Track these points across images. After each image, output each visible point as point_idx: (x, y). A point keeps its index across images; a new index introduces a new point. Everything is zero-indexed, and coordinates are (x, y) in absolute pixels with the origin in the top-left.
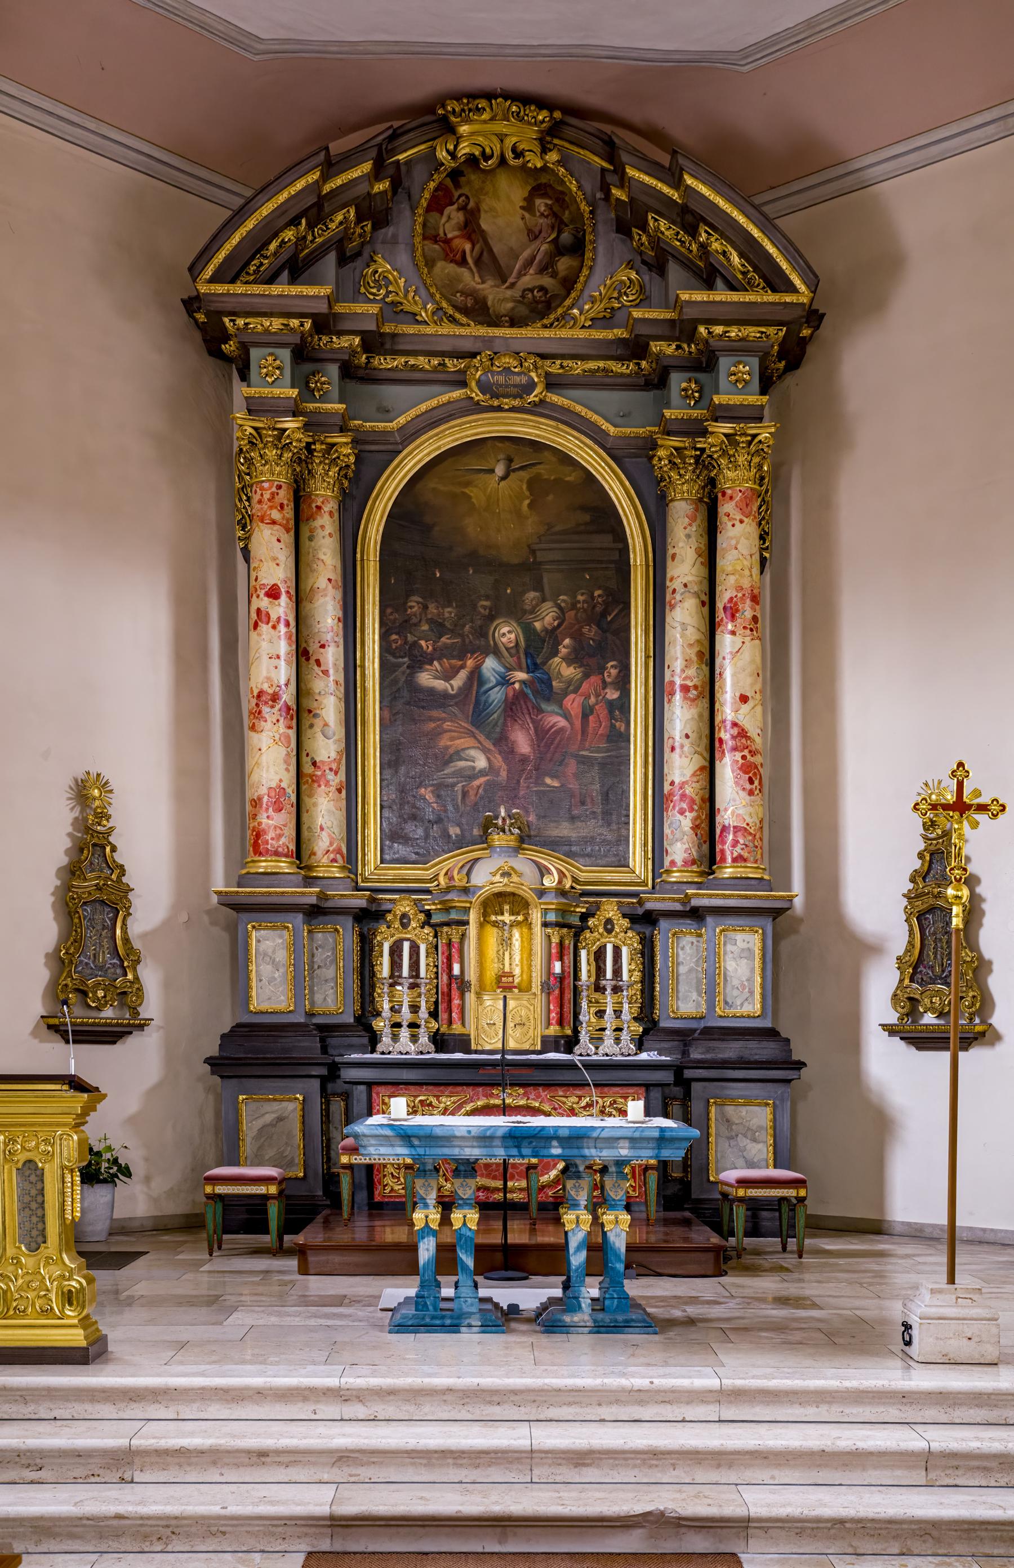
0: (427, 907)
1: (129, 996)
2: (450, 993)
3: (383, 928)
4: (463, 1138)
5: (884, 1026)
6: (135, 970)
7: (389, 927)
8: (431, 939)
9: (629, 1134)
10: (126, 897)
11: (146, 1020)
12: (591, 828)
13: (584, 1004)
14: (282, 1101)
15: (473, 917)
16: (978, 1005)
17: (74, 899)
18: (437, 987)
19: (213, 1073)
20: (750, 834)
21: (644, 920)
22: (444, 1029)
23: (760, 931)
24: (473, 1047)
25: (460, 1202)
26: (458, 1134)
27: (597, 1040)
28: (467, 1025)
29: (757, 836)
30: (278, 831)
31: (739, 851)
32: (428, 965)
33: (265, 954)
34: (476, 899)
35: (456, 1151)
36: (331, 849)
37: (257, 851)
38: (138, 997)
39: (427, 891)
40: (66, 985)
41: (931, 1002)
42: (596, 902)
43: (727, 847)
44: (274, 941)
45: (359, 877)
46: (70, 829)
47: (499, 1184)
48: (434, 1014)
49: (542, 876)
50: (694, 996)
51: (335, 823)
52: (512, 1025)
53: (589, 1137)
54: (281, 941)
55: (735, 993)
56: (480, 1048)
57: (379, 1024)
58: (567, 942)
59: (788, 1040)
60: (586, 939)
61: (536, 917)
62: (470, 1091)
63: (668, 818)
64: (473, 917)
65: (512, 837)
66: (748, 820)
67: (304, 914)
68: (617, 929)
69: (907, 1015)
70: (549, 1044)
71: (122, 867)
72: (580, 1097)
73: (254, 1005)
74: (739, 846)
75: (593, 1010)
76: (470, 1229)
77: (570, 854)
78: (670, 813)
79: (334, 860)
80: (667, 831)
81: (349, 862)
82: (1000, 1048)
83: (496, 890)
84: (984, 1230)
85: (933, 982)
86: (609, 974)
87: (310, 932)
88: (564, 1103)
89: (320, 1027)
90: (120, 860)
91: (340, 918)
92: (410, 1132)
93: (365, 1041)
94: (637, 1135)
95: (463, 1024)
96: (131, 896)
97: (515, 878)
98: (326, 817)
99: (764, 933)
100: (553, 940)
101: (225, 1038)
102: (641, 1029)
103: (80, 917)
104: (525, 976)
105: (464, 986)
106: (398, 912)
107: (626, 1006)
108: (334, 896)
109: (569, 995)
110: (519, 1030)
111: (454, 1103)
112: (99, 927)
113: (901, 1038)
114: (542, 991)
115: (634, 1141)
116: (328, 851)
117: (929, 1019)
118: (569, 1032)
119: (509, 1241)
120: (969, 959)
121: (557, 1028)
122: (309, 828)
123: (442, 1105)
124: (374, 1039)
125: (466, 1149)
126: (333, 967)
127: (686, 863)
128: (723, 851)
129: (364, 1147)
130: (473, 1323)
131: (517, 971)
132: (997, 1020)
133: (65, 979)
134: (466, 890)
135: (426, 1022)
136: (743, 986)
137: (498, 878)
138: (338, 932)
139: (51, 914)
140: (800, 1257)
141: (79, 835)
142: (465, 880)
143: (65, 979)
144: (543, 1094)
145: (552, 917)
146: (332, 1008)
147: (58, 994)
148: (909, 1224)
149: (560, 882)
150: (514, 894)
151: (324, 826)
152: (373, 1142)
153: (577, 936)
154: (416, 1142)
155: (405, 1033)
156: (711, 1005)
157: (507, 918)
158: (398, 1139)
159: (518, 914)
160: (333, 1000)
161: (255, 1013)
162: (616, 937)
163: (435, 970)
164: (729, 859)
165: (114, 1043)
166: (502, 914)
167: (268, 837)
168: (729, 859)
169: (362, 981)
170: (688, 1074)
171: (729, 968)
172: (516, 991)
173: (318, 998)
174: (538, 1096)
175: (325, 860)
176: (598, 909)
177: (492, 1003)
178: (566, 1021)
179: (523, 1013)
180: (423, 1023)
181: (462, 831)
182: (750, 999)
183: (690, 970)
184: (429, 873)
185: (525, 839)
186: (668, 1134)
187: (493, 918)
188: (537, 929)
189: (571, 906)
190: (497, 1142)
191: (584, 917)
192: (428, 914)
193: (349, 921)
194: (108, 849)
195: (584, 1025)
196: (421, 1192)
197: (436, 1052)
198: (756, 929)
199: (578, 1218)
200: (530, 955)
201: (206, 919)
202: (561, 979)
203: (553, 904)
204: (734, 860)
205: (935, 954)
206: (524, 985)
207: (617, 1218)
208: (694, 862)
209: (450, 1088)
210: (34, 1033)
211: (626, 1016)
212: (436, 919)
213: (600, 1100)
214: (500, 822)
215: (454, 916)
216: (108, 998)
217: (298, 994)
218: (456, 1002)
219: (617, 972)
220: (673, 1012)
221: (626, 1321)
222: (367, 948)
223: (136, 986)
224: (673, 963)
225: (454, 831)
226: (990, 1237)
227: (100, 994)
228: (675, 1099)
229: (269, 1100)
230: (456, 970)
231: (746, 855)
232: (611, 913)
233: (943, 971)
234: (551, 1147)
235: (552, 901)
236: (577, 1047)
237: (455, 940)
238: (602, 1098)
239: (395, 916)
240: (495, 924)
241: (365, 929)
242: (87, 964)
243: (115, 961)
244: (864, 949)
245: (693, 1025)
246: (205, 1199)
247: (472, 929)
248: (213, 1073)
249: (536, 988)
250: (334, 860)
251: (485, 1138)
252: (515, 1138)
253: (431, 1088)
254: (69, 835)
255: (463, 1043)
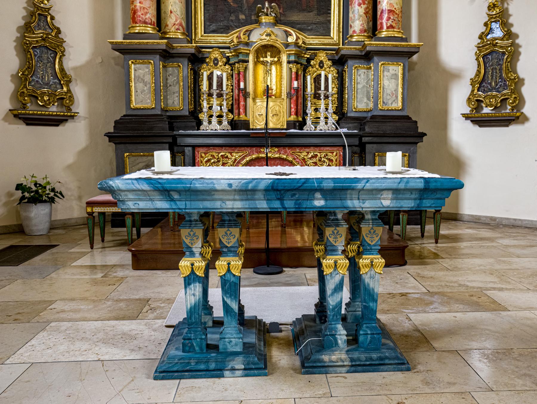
0: (227, 55)
1: (66, 101)
2: (239, 98)
3: (205, 66)
4: (223, 191)
5: (464, 115)
6: (68, 86)
7: (208, 65)
8: (229, 71)
9: (395, 186)
10: (62, 46)
11: (74, 113)
12: (311, 17)
13: (309, 104)
14: (148, 156)
15: (251, 58)
16: (517, 102)
17: (27, 44)
18: (233, 97)
19: (110, 141)
20: (396, 14)
21: (340, 61)
22: (236, 118)
23: (402, 65)
24: (251, 127)
25: (225, 250)
26: (218, 187)
27: (316, 123)
28: (248, 115)
29: (400, 15)
30: (146, 10)
31: (391, 23)
32: (227, 85)
33: (139, 77)
34: (253, 48)
35: (218, 204)
36: (176, 23)
37: (135, 22)
38: (70, 101)
39: (228, 48)
40: (23, 92)
41: (490, 101)
42: (314, 53)
43: (384, 21)
44: (144, 70)
45: (193, 41)
46: (25, 5)
47: (269, 155)
48: (231, 111)
49: (287, 37)
50: (365, 100)
51: (178, 9)
52: (271, 115)
53: (353, 189)
54: (147, 70)
55: (389, 97)
56: (254, 127)
57: (203, 117)
58: (300, 73)
59: (416, 122)
60: (309, 71)
61: (284, 58)
62: (248, 150)
63: (352, 8)
64: (251, 58)
65: (272, 17)
66: (396, 6)
67: (160, 56)
68: (325, 66)
69: (475, 109)
70: (291, 124)
71: (58, 29)
72: (308, 153)
73: (133, 105)
74: (391, 20)
75: (313, 108)
76: (234, 275)
77: (300, 30)
78: (353, 6)
79: (178, 29)
80: (351, 15)
81: (188, 31)
82: (527, 125)
83: (263, 44)
84: (515, 220)
85: (491, 90)
86: (323, 88)
87: (164, 67)
88: (299, 156)
89: (170, 117)
90: (57, 25)
91: (181, 59)
92: (167, 186)
93: (194, 124)
94: (402, 186)
95: (246, 115)
96: (64, 45)
97: (273, 37)
98: (173, 6)
99: (404, 66)
100: (293, 71)
101: (117, 123)
102: (337, 118)
103: (31, 55)
104: (278, 90)
105: (246, 95)
106: (212, 57)
107: (330, 105)
108: (177, 46)
109: (300, 100)
110: (275, 117)
111: (240, 156)
112: (45, 61)
113: (472, 121)
114: (287, 97)
115: (397, 192)
116: (175, 24)
117: (487, 110)
118: (300, 119)
119: (271, 246)
120: (512, 78)
121: (295, 116)
122: (165, 12)
123: (233, 158)
124: (199, 123)
125: (227, 202)
126: (178, 85)
127: (361, 31)
128: (381, 24)
129: (123, 201)
130: (237, 367)
131: (274, 87)
132: (526, 110)
133: (22, 89)
134: (247, 44)
135: (227, 115)
136: (392, 93)
137: (264, 37)
138: (180, 67)
139: (14, 53)
140: (437, 242)
141: (32, 9)
142: (247, 39)
143: (22, 89)
144: (288, 151)
145: (292, 58)
146: (177, 108)
147: (19, 96)
148: (472, 216)
149: (297, 40)
150: (272, 46)
151: (172, 10)
152: (131, 196)
153: (304, 71)
154: (176, 196)
155: (214, 120)
156: (376, 104)
157: (269, 59)
158: (155, 193)
159: (275, 57)
160: (178, 102)
161: (134, 109)
162: (325, 70)
163: (231, 88)
164: (385, 27)
165: (58, 125)
166: (267, 57)
167: (139, 13)
168: (385, 27)
169: (195, 94)
170: (365, 139)
171: (385, 84)
172: (274, 97)
173: (170, 102)
174: (286, 152)
175: (173, 29)
176: (316, 56)
177: (261, 104)
178: (299, 114)
179: (277, 109)
180: (225, 114)
181: (246, 16)
182: (396, 101)
183: (364, 87)
184: (228, 40)
185: (277, 22)
186: (432, 185)
187: (262, 59)
188: (285, 64)
189: (302, 53)
190: (260, 195)
191: (309, 60)
192: (228, 58)
193: (186, 61)
194: (49, 19)
195: (309, 115)
196: (187, 241)
197: (232, 129)
198: (400, 63)
199: (336, 262)
200: (281, 78)
201: (112, 62)
202: (297, 90)
203: (293, 51)
204: (388, 28)
205: (492, 76)
206: (278, 95)
207: (372, 262)
208: (365, 31)
209: (238, 148)
210: (5, 119)
211: (331, 110)
212: (232, 61)
213: (319, 154)
214: (265, 10)
215: (241, 57)
216: (51, 101)
217: (157, 100)
218: (242, 103)
219: (327, 88)
220: (355, 108)
221: (381, 359)
222: (197, 77)
223: (69, 95)
224: (355, 83)
225: (242, 17)
226: (520, 223)
227: (46, 98)
228: (356, 153)
229: (141, 156)
230: (242, 85)
231: (394, 25)
232: (323, 58)
233: (497, 85)
234: (314, 199)
235: (293, 50)
236: (305, 127)
237: (242, 70)
238: (320, 153)
239: (211, 59)
240: (263, 63)
241: (196, 68)
242: (37, 81)
243: (56, 81)
244: (451, 76)
245: (365, 115)
246: (87, 216)
247: (251, 65)
248: (110, 141)
249: (284, 96)
250: (178, 29)
251: (247, 191)
252: (277, 189)
253: (227, 148)
254: (24, 8)
255: (246, 125)
